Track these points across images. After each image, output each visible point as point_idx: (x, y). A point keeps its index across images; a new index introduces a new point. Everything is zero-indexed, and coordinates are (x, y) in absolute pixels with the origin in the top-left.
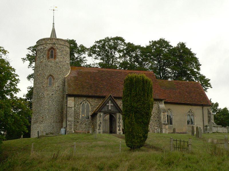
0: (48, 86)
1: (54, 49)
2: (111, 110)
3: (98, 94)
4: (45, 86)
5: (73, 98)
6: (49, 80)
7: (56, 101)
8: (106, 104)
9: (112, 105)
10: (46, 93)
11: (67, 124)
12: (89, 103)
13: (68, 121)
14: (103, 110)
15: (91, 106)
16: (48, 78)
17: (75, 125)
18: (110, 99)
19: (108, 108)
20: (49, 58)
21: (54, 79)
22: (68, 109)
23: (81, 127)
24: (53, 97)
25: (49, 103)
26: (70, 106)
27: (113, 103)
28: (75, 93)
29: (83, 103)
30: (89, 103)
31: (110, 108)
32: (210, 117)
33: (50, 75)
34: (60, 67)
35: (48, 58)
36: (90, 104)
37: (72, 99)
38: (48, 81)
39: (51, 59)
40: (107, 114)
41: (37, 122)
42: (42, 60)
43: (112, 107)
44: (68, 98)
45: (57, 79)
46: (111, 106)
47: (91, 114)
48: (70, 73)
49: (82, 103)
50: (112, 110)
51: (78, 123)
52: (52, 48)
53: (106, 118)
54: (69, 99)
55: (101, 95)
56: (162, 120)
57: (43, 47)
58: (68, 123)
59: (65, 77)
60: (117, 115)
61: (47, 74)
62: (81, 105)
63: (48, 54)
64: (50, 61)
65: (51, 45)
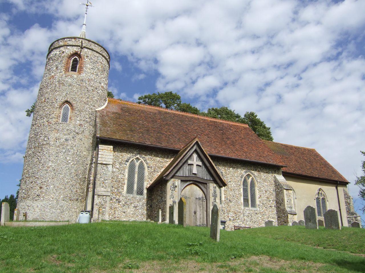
0: (60, 122)
1: (79, 56)
2: (198, 176)
3: (164, 145)
4: (53, 121)
5: (112, 147)
6: (62, 111)
7: (73, 154)
8: (186, 161)
9: (200, 163)
10: (53, 136)
11: (95, 203)
12: (143, 161)
13: (96, 197)
14: (180, 173)
15: (148, 167)
16: (61, 107)
17: (111, 208)
18: (196, 151)
19: (191, 170)
20: (69, 71)
21: (73, 109)
22: (99, 166)
23: (124, 213)
24: (67, 145)
25: (57, 156)
26: (104, 163)
27: (202, 160)
28: (117, 137)
29: (132, 160)
30: (145, 161)
31: (195, 171)
32: (349, 204)
33: (67, 102)
34: (87, 88)
35: (67, 70)
36: (147, 163)
37: (109, 149)
38: (62, 113)
39: (71, 73)
40: (188, 183)
41: (29, 196)
42: (53, 74)
43: (200, 169)
44: (100, 146)
45: (80, 111)
46: (197, 165)
47: (147, 184)
48: (106, 107)
49: (130, 161)
50: (200, 175)
51: (119, 202)
52: (76, 54)
53: (187, 193)
54: (101, 147)
55: (171, 147)
56: (286, 206)
57: (59, 51)
58: (97, 200)
59: (97, 110)
60: (209, 188)
61: (61, 99)
62: (128, 164)
63: (67, 64)
64: (69, 75)
65: (75, 49)
